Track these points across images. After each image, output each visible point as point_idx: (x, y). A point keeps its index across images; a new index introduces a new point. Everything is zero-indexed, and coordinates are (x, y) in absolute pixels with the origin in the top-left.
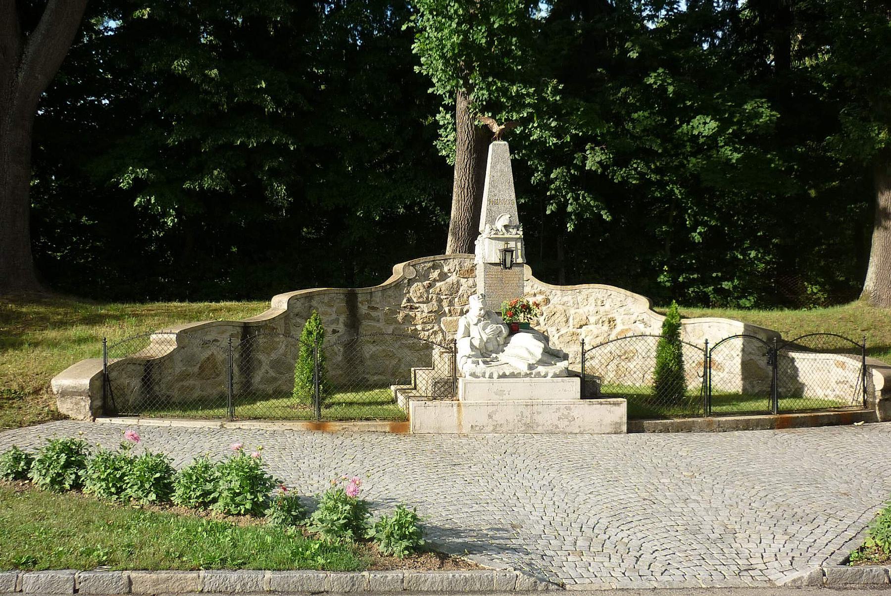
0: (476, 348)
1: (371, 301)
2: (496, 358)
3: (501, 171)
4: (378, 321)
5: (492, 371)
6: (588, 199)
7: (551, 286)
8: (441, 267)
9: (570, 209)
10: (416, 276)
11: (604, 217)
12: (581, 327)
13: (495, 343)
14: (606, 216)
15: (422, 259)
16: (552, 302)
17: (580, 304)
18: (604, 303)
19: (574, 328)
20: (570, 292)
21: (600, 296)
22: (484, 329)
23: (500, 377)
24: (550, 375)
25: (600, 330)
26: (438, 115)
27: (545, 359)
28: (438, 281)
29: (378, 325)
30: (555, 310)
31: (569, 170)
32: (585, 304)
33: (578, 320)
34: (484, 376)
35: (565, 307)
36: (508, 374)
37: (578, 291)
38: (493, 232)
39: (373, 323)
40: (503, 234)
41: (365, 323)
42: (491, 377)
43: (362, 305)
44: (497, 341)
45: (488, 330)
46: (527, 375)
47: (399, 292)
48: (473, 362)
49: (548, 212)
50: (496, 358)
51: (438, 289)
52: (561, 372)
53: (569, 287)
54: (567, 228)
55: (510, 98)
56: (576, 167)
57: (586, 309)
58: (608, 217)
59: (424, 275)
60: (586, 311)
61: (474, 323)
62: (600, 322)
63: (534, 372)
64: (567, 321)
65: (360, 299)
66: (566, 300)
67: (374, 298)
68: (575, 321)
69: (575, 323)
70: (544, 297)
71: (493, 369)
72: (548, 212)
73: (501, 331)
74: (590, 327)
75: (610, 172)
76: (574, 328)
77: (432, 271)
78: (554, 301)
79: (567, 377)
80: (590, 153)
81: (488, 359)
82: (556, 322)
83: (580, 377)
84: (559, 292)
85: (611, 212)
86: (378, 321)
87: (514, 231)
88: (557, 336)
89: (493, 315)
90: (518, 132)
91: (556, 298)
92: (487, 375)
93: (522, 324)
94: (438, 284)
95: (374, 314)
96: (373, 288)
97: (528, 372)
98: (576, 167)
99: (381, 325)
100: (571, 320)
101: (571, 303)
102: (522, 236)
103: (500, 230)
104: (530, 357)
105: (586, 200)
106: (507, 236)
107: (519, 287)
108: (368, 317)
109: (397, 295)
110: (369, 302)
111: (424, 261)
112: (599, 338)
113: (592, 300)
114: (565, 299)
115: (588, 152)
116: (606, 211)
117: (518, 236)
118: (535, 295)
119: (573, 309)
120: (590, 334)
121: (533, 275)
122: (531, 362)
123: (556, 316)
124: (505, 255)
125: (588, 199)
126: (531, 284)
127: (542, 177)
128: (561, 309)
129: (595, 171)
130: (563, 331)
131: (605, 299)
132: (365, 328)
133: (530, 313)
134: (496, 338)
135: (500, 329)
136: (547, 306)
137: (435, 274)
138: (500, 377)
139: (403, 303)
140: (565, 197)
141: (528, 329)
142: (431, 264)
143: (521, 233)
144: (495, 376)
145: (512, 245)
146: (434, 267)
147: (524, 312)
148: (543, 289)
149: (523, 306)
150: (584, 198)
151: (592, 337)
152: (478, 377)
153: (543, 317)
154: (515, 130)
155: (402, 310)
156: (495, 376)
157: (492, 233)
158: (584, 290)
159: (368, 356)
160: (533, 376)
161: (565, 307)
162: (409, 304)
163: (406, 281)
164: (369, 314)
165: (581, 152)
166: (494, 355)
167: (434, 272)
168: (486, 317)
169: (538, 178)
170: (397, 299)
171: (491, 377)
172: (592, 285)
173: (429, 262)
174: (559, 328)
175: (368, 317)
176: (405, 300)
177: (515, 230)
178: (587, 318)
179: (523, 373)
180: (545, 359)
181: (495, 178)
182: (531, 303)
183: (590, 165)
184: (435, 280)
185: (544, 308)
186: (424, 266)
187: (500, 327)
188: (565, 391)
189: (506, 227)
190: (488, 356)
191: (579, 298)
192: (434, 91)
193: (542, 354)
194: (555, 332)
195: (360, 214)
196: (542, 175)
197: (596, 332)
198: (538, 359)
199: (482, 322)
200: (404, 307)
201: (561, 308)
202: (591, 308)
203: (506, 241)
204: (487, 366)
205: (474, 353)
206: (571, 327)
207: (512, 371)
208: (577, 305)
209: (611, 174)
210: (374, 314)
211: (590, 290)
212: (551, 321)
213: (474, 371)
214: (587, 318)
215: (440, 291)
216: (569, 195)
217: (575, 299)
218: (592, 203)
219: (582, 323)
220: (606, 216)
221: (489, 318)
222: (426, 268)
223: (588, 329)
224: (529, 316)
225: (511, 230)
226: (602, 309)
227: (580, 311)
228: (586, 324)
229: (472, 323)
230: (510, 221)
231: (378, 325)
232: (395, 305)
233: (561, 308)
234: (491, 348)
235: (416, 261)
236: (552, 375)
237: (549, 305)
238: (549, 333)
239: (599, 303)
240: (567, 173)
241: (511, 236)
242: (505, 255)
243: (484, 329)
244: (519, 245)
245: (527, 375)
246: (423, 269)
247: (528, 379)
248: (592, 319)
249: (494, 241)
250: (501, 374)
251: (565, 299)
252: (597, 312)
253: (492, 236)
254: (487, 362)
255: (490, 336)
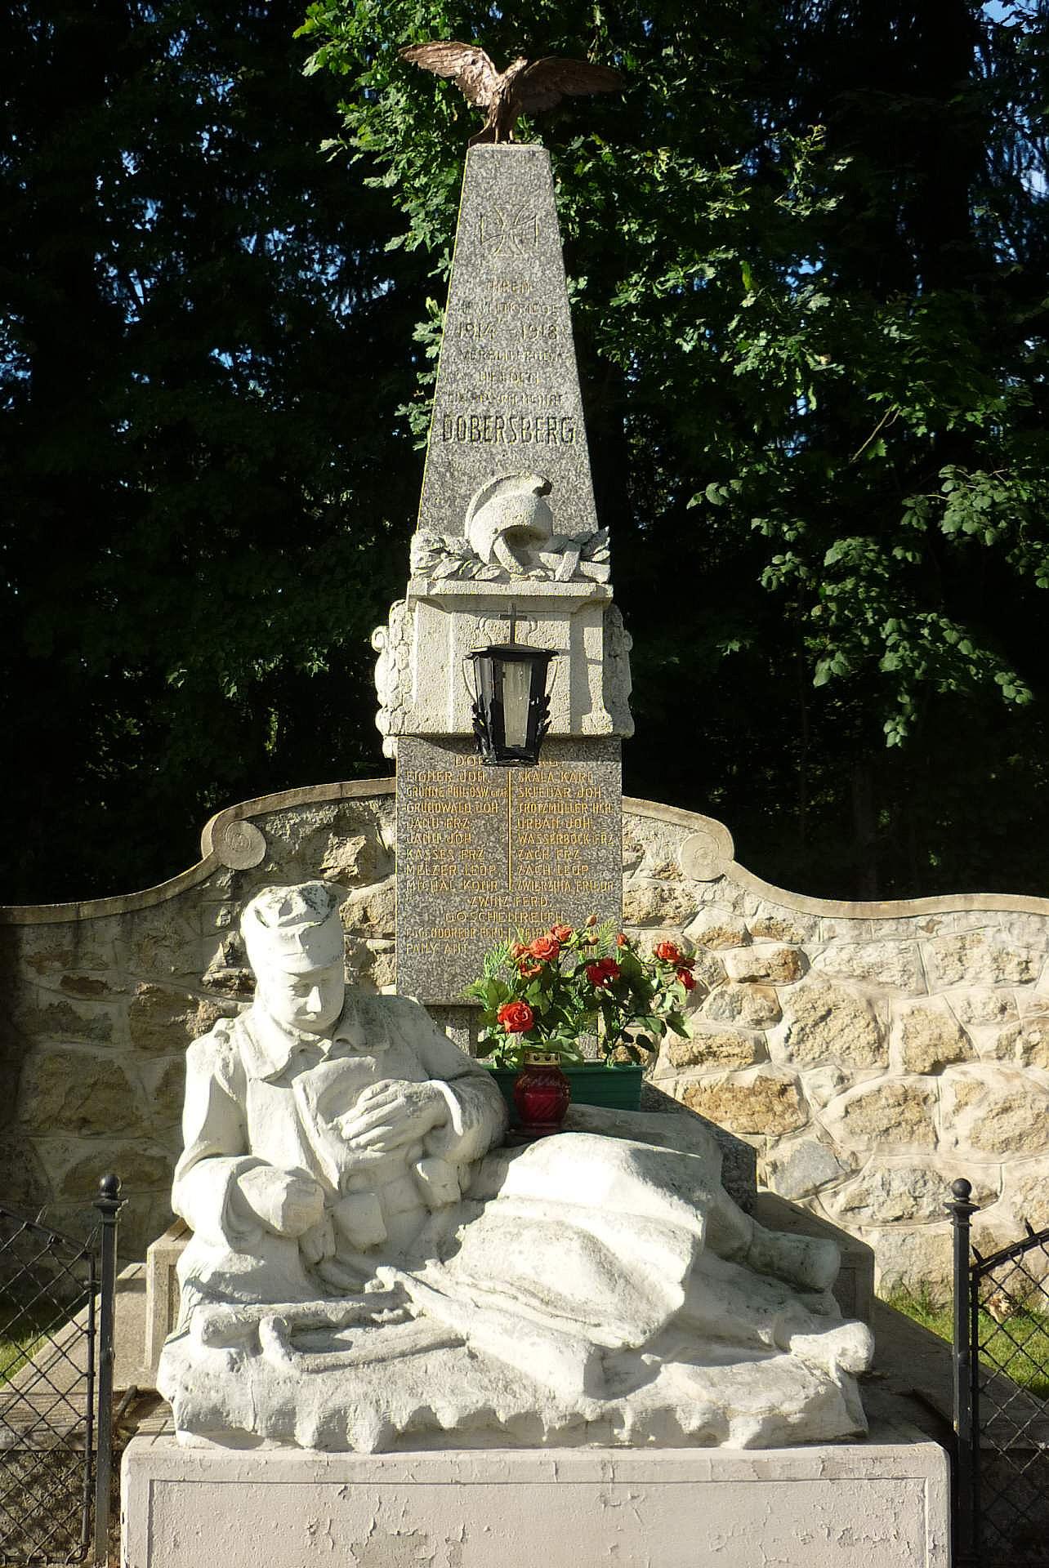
0: (268, 1231)
1: (77, 959)
2: (398, 1296)
3: (512, 281)
4: (105, 1037)
5: (337, 1401)
6: (951, 636)
7: (815, 905)
8: (370, 826)
9: (890, 663)
10: (267, 859)
11: (1008, 692)
12: (937, 1068)
13: (404, 1198)
14: (1012, 691)
15: (293, 796)
16: (816, 966)
17: (932, 976)
18: (1033, 973)
19: (907, 1072)
20: (888, 927)
21: (1012, 942)
22: (331, 1106)
23: (393, 1440)
24: (742, 1430)
25: (1017, 1082)
26: (419, 326)
27: (713, 1311)
28: (357, 881)
29: (101, 1052)
30: (830, 998)
31: (886, 549)
32: (952, 974)
33: (924, 1038)
34: (283, 1434)
35: (870, 989)
36: (447, 1419)
37: (922, 921)
38: (445, 567)
39: (83, 1047)
40: (504, 578)
41: (50, 1043)
42: (332, 1437)
43: (40, 971)
44: (417, 1183)
45: (353, 1121)
46: (577, 1431)
47: (195, 923)
48: (216, 1336)
49: (819, 681)
50: (398, 1296)
51: (357, 914)
52: (815, 1406)
53: (885, 905)
54: (885, 736)
55: (648, 209)
56: (909, 538)
57: (958, 994)
58: (1019, 692)
59: (301, 858)
60: (959, 1005)
61: (268, 1070)
62: (1019, 1048)
63: (631, 1407)
64: (879, 1044)
65: (28, 949)
66: (872, 960)
67: (89, 946)
68: (914, 1043)
69: (913, 1053)
70: (782, 946)
71: (350, 1389)
72: (819, 681)
73: (441, 1126)
74: (974, 1070)
75: (1021, 556)
76: (907, 1072)
77: (333, 840)
78: (825, 960)
79: (859, 1438)
80: (954, 490)
81: (334, 1310)
82: (836, 1047)
83: (942, 1433)
84: (844, 929)
85: (1027, 675)
86: (105, 1037)
87: (563, 564)
88: (837, 1105)
89: (407, 1025)
90: (687, 348)
91: (831, 952)
92: (306, 1431)
93: (596, 1072)
94: (357, 894)
95: (87, 1009)
96: (87, 909)
97: (590, 1409)
98: (909, 538)
99: (117, 1053)
100: (895, 1038)
101: (893, 974)
102: (610, 591)
103: (485, 558)
104: (605, 1299)
105: (944, 641)
106: (522, 586)
107: (593, 865)
108: (63, 1020)
109: (189, 935)
110: (70, 959)
111: (298, 801)
112: (1015, 1117)
113: (979, 956)
114: (870, 955)
115: (947, 487)
116: (1012, 675)
117: (583, 590)
118: (747, 939)
119: (905, 994)
120: (975, 1098)
121: (738, 858)
122: (614, 1336)
123: (835, 1023)
124: (498, 677)
125: (951, 636)
126: (731, 894)
127: (797, 568)
128: (856, 996)
129: (974, 536)
130: (859, 1089)
131: (1034, 954)
132: (50, 1067)
133: (641, 1009)
134: (411, 1166)
135: (428, 1116)
136: (798, 985)
137: (343, 855)
138: (393, 1440)
139: (213, 966)
140: (873, 632)
141: (631, 1106)
142: (327, 815)
143: (602, 574)
144: (363, 1433)
145: (551, 634)
146: (342, 827)
147: (607, 1005)
148: (779, 915)
149: (599, 970)
150: (935, 628)
151: (981, 1113)
152: (242, 1440)
153: (782, 1029)
154: (678, 341)
155: (205, 995)
156: (363, 1433)
157: (441, 571)
158: (944, 918)
159: (55, 1175)
160: (624, 1434)
161: (870, 989)
162: (235, 971)
163: (224, 880)
164: (66, 1009)
165: (925, 490)
166: (387, 1276)
167: (340, 845)
168: (353, 1032)
169: (784, 569)
170: (187, 949)
171: (332, 1437)
172: (980, 899)
173: (320, 805)
174: (846, 1072)
175: (63, 1020)
176: (220, 955)
177: (570, 558)
178: (962, 1032)
179: (550, 1418)
180: (713, 1311)
181: (475, 313)
182: (646, 954)
183: (957, 518)
184: (344, 880)
185: (785, 993)
186: (303, 823)
187: (440, 1095)
188: (846, 1538)
189: (518, 539)
190: (346, 1280)
191: (928, 950)
192: (403, 244)
193: (695, 1278)
194: (828, 1089)
195: (176, 680)
196: (797, 560)
197: (999, 1090)
198: (660, 1317)
199: (322, 1067)
200: (218, 984)
201: (852, 989)
202: (979, 993)
203: (517, 609)
204: (313, 1360)
205: (248, 1264)
206: (897, 1069)
207: (475, 1399)
208: (919, 980)
209: (1023, 562)
210: (87, 1009)
211: (973, 917)
212: (814, 1045)
213: (215, 1399)
214: (962, 1032)
215: (365, 918)
216: (889, 625)
217: (909, 956)
218: (964, 648)
219: (944, 1052)
220: (1012, 691)
221: (369, 1042)
222: (308, 830)
223: (968, 1080)
224: (635, 1030)
225: (545, 557)
226: (1023, 996)
227: (935, 1003)
228: (959, 1059)
229: (255, 1071)
230: (542, 511)
231: (101, 1052)
232: (179, 975)
233: (851, 989)
234: (366, 1222)
235: (270, 801)
236: (754, 1428)
237: (807, 980)
238: (807, 1093)
239: (1012, 971)
240: (879, 553)
241: (547, 589)
242: (498, 677)
243: (331, 1106)
244: (593, 638)
245: (577, 1431)
246: (294, 833)
247: (585, 1457)
248: (984, 1038)
249: (451, 618)
250: (400, 1420)
251: (870, 955)
252: (1003, 1009)
253: (440, 587)
254: (330, 1327)
255: (370, 1153)
